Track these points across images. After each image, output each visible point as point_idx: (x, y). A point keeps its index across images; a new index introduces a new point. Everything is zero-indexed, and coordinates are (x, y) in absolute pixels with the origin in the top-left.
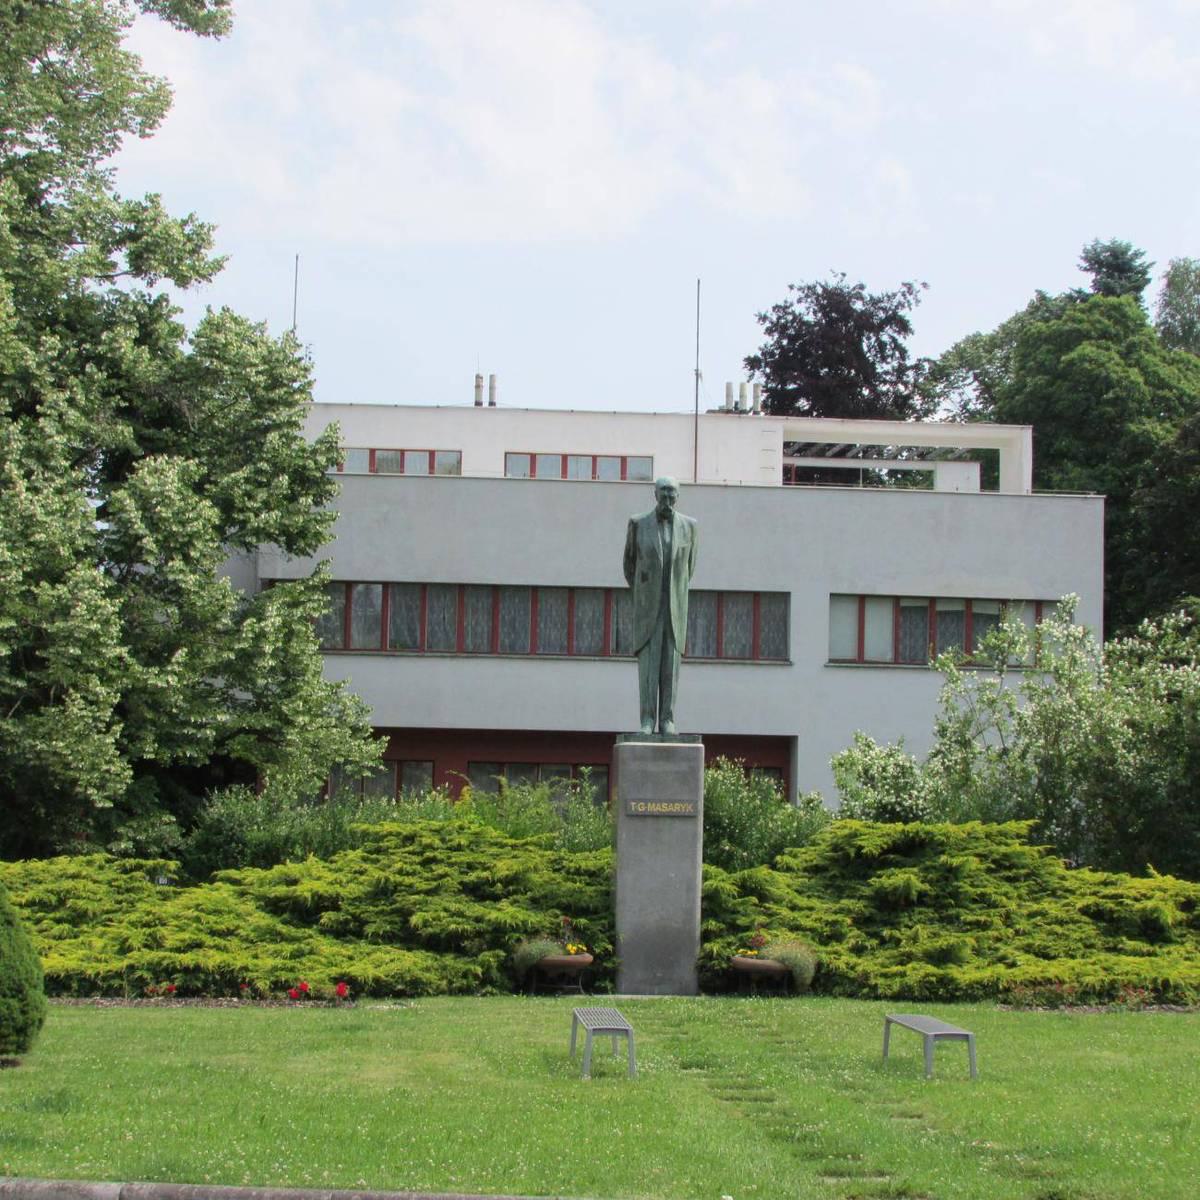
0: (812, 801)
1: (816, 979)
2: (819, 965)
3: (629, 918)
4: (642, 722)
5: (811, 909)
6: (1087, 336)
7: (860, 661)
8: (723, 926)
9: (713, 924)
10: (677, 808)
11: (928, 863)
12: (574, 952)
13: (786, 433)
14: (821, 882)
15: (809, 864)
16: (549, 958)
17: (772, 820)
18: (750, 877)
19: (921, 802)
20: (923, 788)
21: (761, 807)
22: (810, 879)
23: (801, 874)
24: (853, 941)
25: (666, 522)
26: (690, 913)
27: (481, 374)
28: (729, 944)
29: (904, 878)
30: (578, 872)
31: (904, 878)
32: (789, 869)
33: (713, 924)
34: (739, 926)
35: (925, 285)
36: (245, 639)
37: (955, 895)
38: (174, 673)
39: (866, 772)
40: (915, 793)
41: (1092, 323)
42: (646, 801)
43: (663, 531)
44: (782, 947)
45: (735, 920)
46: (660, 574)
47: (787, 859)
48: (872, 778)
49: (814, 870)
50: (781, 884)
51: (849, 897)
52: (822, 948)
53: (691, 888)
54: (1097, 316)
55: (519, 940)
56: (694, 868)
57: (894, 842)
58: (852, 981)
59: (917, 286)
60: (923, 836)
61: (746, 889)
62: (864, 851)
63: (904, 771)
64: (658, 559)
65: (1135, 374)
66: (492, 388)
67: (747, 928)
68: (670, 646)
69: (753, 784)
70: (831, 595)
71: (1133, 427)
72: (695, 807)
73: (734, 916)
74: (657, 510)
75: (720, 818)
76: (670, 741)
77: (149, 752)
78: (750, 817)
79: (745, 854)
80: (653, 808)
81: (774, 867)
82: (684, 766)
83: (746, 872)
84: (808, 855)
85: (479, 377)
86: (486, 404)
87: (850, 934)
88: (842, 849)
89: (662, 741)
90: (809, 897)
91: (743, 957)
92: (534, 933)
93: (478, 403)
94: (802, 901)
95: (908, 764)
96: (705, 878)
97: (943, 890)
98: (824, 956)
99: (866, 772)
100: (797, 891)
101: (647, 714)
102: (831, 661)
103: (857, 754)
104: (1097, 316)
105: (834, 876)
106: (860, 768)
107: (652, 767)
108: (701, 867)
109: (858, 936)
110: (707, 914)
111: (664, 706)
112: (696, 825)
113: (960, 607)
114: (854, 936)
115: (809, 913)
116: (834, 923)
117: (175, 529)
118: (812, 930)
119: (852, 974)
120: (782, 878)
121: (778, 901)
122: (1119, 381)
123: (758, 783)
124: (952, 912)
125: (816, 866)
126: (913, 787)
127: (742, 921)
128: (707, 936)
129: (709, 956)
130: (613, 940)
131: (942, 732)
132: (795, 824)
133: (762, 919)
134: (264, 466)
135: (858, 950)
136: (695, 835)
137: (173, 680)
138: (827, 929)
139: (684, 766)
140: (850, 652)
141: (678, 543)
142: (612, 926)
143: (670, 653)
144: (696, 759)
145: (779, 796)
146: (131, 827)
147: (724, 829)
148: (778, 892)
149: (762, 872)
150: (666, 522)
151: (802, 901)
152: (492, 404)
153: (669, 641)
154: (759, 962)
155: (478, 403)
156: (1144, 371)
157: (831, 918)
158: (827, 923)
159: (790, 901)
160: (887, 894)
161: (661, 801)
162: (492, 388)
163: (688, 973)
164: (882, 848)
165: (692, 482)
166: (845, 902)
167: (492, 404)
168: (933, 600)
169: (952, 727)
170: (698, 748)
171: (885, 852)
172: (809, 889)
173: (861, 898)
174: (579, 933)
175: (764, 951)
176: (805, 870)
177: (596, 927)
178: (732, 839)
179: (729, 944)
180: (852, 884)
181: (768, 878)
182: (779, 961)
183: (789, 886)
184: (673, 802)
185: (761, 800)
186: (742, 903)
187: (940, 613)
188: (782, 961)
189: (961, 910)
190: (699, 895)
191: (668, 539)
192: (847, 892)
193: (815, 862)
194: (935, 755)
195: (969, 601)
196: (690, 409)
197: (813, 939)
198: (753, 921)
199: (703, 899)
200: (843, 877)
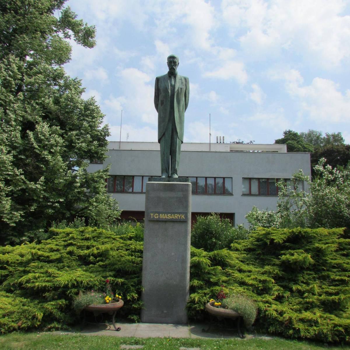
0: (241, 227)
1: (257, 320)
2: (259, 311)
3: (150, 279)
4: (162, 173)
5: (250, 271)
6: (289, 139)
7: (250, 194)
8: (201, 283)
9: (196, 282)
10: (176, 216)
11: (307, 247)
12: (110, 301)
13: (230, 148)
14: (253, 257)
15: (246, 247)
16: (92, 306)
17: (229, 232)
18: (218, 254)
19: (277, 226)
20: (277, 221)
21: (225, 228)
22: (247, 254)
23: (243, 252)
24: (276, 293)
26: (184, 276)
28: (205, 294)
29: (298, 256)
31: (298, 256)
32: (237, 250)
33: (196, 282)
34: (211, 282)
35: (254, 141)
36: (68, 176)
37: (325, 263)
38: (39, 184)
39: (257, 218)
40: (275, 223)
41: (290, 137)
42: (159, 213)
43: (171, 81)
44: (238, 301)
45: (209, 278)
46: (169, 99)
47: (236, 245)
48: (259, 220)
49: (248, 250)
50: (233, 257)
51: (268, 265)
52: (260, 298)
53: (184, 261)
54: (291, 136)
55: (77, 294)
56: (185, 250)
57: (288, 237)
58: (281, 323)
59: (253, 141)
60: (304, 234)
61: (216, 261)
62: (275, 241)
63: (271, 216)
64: (168, 92)
65: (300, 146)
66: (223, 139)
67: (216, 284)
68: (175, 136)
69: (223, 221)
70: (243, 178)
72: (186, 216)
73: (209, 276)
75: (212, 231)
76: (173, 181)
77: (32, 209)
78: (222, 231)
79: (220, 243)
80: (163, 216)
81: (230, 248)
82: (180, 194)
83: (216, 252)
84: (241, 245)
85: (217, 137)
86: (222, 142)
87: (274, 289)
88: (263, 240)
89: (169, 181)
90: (248, 264)
91: (214, 306)
92: (89, 288)
93: (217, 142)
94: (245, 267)
95: (272, 214)
96: (193, 255)
97: (318, 262)
98: (261, 304)
99: (257, 218)
100: (242, 261)
101: (165, 169)
102: (243, 194)
103: (254, 213)
104: (291, 136)
105: (259, 254)
106: (255, 217)
107: (163, 195)
108: (190, 249)
109: (279, 290)
110: (193, 276)
111: (173, 166)
112: (187, 227)
114: (276, 289)
115: (249, 274)
116: (264, 282)
117: (46, 143)
118: (252, 285)
119: (281, 319)
120: (234, 254)
121: (232, 267)
122: (297, 147)
123: (224, 221)
124: (325, 273)
125: (249, 248)
126: (274, 221)
127: (213, 279)
128: (193, 289)
129: (193, 302)
130: (139, 293)
131: (280, 206)
132: (236, 233)
133: (224, 278)
134: (83, 132)
135: (279, 299)
136: (186, 231)
137: (39, 186)
138: (260, 285)
139: (180, 194)
140: (248, 192)
141: (178, 86)
142: (140, 283)
143: (175, 140)
144: (187, 191)
145: (231, 225)
146: (30, 233)
147: (213, 235)
148: (233, 262)
149: (225, 252)
151: (245, 267)
153: (175, 133)
154: (222, 310)
155: (217, 142)
156: (301, 145)
157: (263, 278)
158: (260, 281)
159: (239, 267)
160: (291, 264)
161: (167, 213)
162: (223, 139)
163: (182, 313)
164: (283, 240)
165: (208, 150)
166: (267, 268)
168: (268, 179)
169: (283, 204)
170: (188, 184)
171: (285, 242)
172: (247, 259)
173: (274, 265)
174: (115, 288)
175: (226, 301)
176: (245, 250)
177: (130, 283)
178: (216, 238)
179: (205, 294)
180: (268, 257)
181: (227, 255)
182: (235, 311)
183: (237, 258)
184: (174, 213)
185: (225, 226)
186: (214, 269)
187: (270, 182)
188: (236, 310)
189: (330, 273)
190: (189, 265)
191: (173, 83)
192: (267, 262)
193: (249, 247)
194: (279, 212)
196: (208, 142)
197: (253, 291)
198: (219, 280)
199: (191, 267)
200: (263, 254)
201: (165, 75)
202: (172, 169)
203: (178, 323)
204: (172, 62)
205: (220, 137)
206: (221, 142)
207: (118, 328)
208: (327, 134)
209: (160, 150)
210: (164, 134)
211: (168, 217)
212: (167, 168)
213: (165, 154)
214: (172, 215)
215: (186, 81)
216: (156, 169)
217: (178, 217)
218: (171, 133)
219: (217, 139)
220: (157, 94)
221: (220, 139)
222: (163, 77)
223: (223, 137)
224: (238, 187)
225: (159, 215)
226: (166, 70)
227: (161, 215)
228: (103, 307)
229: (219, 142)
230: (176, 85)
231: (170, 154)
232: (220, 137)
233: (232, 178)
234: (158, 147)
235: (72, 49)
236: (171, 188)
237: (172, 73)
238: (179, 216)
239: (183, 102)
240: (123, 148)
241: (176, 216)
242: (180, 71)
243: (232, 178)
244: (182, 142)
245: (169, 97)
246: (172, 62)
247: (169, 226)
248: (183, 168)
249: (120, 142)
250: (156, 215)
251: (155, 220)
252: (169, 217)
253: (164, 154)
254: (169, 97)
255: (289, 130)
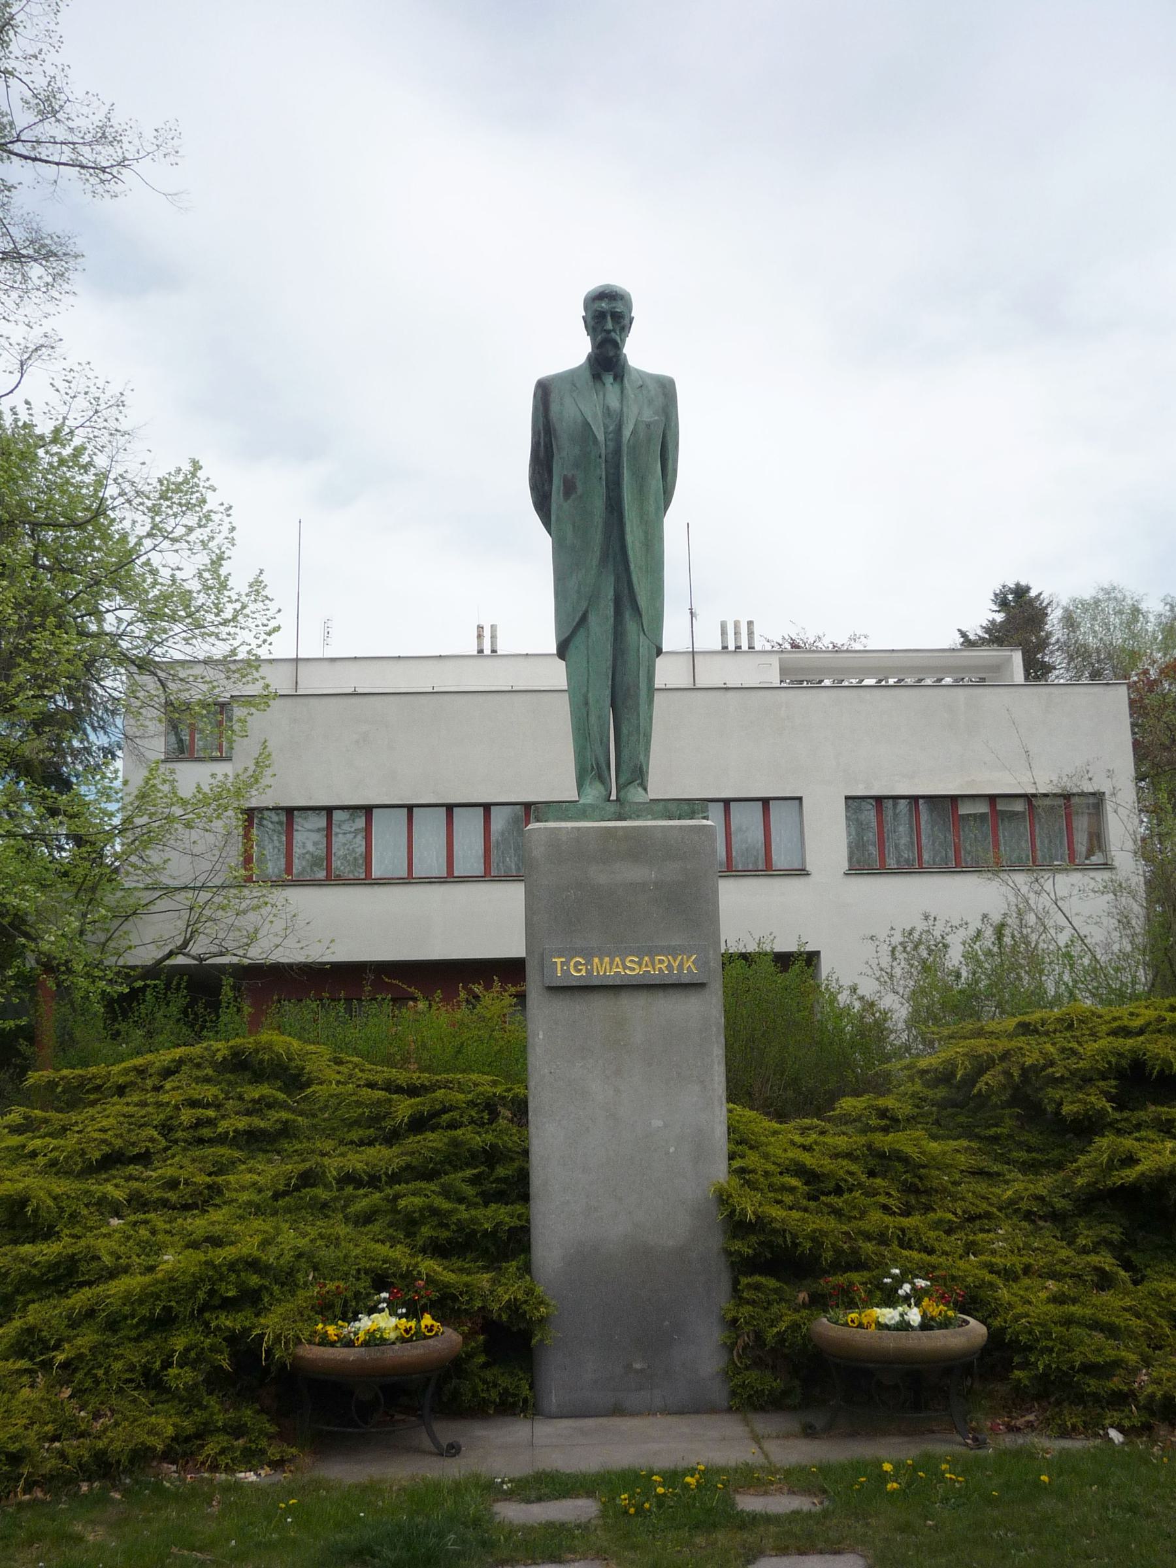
25: (609, 379)
27: (482, 623)
30: (121, 1090)
42: (588, 955)
66: (751, 634)
70: (847, 798)
71: (1150, 627)
74: (589, 357)
80: (607, 968)
86: (487, 651)
93: (481, 651)
101: (590, 769)
111: (626, 754)
113: (983, 808)
150: (609, 379)
152: (494, 651)
155: (481, 651)
162: (751, 634)
165: (686, 682)
167: (494, 651)
184: (652, 952)
195: (992, 799)
201: (581, 366)
202: (624, 767)
203: (695, 1407)
204: (608, 316)
205: (737, 625)
206: (738, 647)
207: (451, 1446)
208: (1169, 600)
209: (563, 684)
210: (584, 619)
211: (625, 967)
212: (604, 767)
213: (591, 701)
214: (641, 959)
215: (666, 390)
216: (542, 764)
217: (669, 967)
218: (611, 612)
219: (724, 633)
220: (542, 454)
221: (737, 633)
222: (569, 378)
223: (750, 623)
224: (827, 837)
225: (589, 962)
226: (575, 349)
227: (596, 960)
228: (416, 1352)
229: (732, 647)
230: (625, 409)
231: (613, 705)
232: (737, 625)
233: (800, 799)
234: (557, 675)
235: (637, 312)
236: (638, 848)
237: (607, 360)
238: (675, 965)
239: (655, 482)
240: (312, 682)
241: (661, 962)
242: (640, 352)
243: (800, 799)
244: (659, 652)
245: (600, 465)
246: (608, 316)
247: (634, 1007)
248: (683, 759)
249: (297, 660)
250: (578, 963)
251: (574, 984)
252: (633, 969)
253: (587, 704)
254: (600, 465)
255: (1018, 585)
